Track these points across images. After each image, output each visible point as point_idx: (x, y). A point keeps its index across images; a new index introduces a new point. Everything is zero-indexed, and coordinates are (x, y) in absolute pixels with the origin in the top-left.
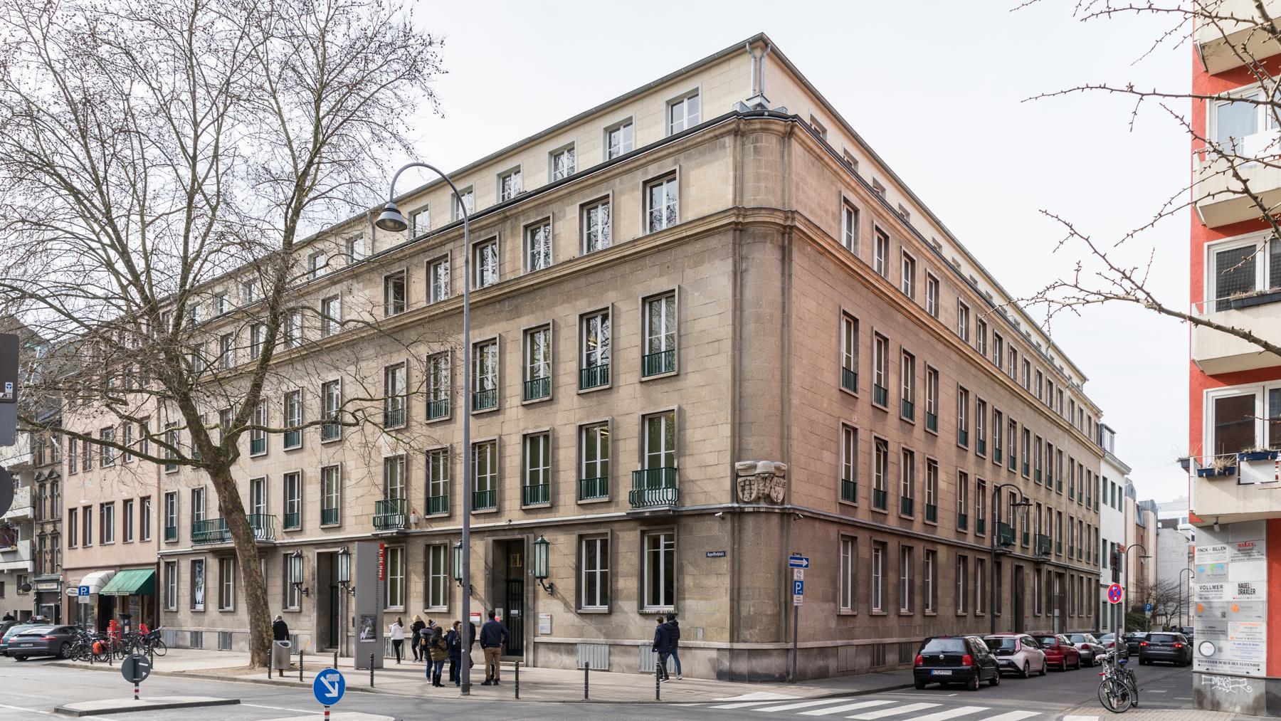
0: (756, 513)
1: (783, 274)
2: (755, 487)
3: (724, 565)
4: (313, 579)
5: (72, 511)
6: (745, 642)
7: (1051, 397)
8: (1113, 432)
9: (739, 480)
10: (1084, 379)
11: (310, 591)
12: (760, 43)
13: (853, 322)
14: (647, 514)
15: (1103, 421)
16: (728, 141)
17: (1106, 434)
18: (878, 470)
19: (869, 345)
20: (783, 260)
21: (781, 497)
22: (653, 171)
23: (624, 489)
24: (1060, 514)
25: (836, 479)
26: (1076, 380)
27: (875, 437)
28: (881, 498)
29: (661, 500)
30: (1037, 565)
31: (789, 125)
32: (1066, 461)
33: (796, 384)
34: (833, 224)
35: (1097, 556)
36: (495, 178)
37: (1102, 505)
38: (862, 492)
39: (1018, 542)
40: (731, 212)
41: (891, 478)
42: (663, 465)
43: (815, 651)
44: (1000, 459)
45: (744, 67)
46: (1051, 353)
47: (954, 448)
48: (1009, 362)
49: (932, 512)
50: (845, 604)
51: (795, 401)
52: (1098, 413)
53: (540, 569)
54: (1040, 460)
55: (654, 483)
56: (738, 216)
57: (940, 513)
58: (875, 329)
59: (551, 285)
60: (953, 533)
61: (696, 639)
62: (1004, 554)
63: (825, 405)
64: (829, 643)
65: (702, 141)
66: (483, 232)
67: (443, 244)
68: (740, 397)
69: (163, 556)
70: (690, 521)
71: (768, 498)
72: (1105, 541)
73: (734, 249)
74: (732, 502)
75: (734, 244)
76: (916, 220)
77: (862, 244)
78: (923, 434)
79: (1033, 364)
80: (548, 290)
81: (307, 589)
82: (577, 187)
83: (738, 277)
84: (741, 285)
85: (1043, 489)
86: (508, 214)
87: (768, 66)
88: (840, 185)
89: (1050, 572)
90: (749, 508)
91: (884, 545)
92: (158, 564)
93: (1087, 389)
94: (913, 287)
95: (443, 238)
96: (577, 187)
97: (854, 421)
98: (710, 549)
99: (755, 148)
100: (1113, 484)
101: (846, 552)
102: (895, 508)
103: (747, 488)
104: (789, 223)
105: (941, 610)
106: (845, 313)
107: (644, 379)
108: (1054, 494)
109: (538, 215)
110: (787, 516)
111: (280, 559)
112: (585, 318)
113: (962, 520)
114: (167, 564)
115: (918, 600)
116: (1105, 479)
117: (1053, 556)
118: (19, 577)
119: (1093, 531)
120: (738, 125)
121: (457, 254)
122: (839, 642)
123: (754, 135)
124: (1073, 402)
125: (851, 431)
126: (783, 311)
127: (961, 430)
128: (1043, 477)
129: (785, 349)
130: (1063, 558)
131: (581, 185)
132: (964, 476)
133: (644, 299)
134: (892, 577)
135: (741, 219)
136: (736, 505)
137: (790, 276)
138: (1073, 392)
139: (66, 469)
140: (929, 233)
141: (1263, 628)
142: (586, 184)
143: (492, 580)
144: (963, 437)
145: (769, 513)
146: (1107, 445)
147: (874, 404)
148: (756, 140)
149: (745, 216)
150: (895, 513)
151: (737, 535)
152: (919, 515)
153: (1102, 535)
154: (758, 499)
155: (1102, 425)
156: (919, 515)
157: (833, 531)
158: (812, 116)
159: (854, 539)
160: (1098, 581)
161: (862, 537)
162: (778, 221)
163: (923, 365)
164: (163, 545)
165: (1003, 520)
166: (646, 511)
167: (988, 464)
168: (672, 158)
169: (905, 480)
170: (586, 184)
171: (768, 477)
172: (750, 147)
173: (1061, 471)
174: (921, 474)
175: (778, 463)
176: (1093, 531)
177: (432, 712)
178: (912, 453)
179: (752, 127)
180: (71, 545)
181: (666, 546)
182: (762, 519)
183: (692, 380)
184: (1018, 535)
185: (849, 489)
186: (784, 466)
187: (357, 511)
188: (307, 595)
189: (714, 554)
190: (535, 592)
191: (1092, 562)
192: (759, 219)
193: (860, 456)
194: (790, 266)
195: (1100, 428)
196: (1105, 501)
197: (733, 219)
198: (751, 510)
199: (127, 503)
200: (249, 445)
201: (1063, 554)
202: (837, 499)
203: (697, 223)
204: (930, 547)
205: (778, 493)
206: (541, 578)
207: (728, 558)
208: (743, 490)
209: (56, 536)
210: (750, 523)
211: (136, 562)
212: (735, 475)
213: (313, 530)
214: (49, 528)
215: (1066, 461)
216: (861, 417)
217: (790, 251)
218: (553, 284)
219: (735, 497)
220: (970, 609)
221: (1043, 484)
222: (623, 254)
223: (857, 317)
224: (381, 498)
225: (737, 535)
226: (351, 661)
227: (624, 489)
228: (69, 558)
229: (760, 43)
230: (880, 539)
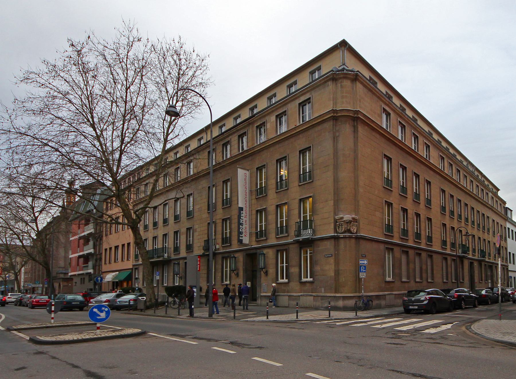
0: (345, 237)
1: (354, 137)
2: (343, 227)
3: (332, 260)
4: (183, 272)
5: (106, 250)
6: (341, 293)
7: (478, 191)
8: (512, 211)
9: (337, 223)
10: (498, 190)
11: (182, 277)
12: (344, 44)
13: (443, 191)
14: (301, 240)
15: (507, 206)
16: (330, 83)
17: (509, 212)
18: (404, 221)
19: (424, 184)
20: (354, 131)
21: (355, 231)
22: (302, 99)
23: (293, 231)
24: (489, 242)
25: (382, 223)
26: (494, 190)
27: (401, 207)
28: (405, 232)
29: (307, 234)
30: (480, 262)
31: (356, 77)
32: (491, 221)
33: (361, 183)
34: (378, 118)
35: (507, 258)
36: (248, 110)
37: (508, 239)
38: (410, 233)
39: (471, 252)
40: (331, 111)
41: (410, 224)
42: (308, 219)
43: (374, 297)
44: (474, 225)
45: (338, 55)
46: (483, 179)
47: (439, 213)
48: (481, 193)
49: (430, 239)
50: (389, 277)
51: (361, 190)
52: (505, 203)
53: (262, 264)
54: (479, 220)
55: (305, 228)
56: (334, 114)
57: (434, 240)
58: (400, 162)
59: (266, 149)
60: (440, 248)
61: (321, 292)
62: (464, 257)
63: (376, 193)
64: (381, 293)
65: (320, 84)
66: (242, 131)
67: (228, 136)
68: (337, 189)
69: (134, 265)
70: (319, 242)
71: (349, 231)
72: (510, 253)
73: (333, 128)
74: (334, 233)
75: (333, 125)
76: (420, 122)
77: (393, 127)
78: (424, 207)
79: (474, 182)
80: (265, 151)
81: (181, 277)
82: (275, 108)
83: (335, 139)
84: (337, 142)
85: (481, 231)
86: (250, 122)
87: (347, 54)
88: (381, 102)
89: (486, 265)
90: (342, 236)
91: (407, 253)
92: (132, 269)
93: (500, 194)
94: (429, 155)
95: (228, 134)
96: (275, 108)
97: (390, 200)
98: (327, 253)
99: (341, 85)
100: (512, 231)
101: (261, 226)
102: (412, 237)
103: (340, 227)
104: (356, 116)
105: (436, 280)
106: (415, 173)
107: (300, 184)
108: (486, 234)
109: (261, 122)
110: (359, 239)
111: (172, 264)
112: (279, 161)
113: (444, 243)
114: (136, 269)
115: (424, 275)
116: (509, 229)
117: (487, 258)
118: (90, 276)
119: (504, 249)
120: (333, 76)
121: (232, 140)
122: (386, 293)
123: (341, 80)
124: (493, 198)
125: (389, 205)
126: (355, 152)
127: (459, 214)
128: (481, 226)
129: (355, 168)
130: (491, 259)
131: (276, 108)
132: (444, 225)
133: (300, 152)
134: (411, 266)
135: (335, 115)
136: (336, 235)
137: (357, 138)
138: (493, 194)
139: (109, 233)
140: (427, 129)
141: (186, 138)
142: (278, 107)
143: (245, 270)
144: (443, 209)
145: (350, 237)
146: (509, 215)
147: (400, 193)
148: (342, 82)
149: (337, 113)
150: (412, 239)
151: (336, 247)
152: (423, 240)
153: (509, 251)
154: (345, 232)
155: (507, 207)
156: (423, 240)
157: (382, 247)
158: (370, 76)
159: (392, 249)
160: (507, 269)
161: (396, 249)
162: (351, 115)
163: (456, 199)
164: (134, 262)
165: (482, 249)
166: (300, 238)
167: (447, 217)
168: (309, 93)
169: (417, 225)
170: (278, 107)
171: (349, 222)
172: (339, 85)
173: (489, 225)
174: (424, 224)
175: (353, 216)
176: (504, 249)
177: (447, 316)
178: (407, 210)
179: (339, 76)
180: (105, 263)
181: (310, 253)
182: (347, 241)
183: (317, 183)
184: (471, 249)
185: (389, 228)
186: (357, 217)
187: (199, 245)
188: (181, 279)
189: (328, 256)
190: (261, 274)
191: (504, 261)
192: (343, 114)
193: (394, 215)
194: (357, 133)
195: (507, 209)
196: (509, 237)
197: (332, 115)
198: (342, 236)
199: (123, 245)
200: (162, 221)
201: (491, 258)
202: (400, 236)
203: (319, 118)
204: (430, 254)
205: (354, 229)
206: (262, 269)
207: (333, 257)
208: (339, 228)
209: (101, 259)
210: (342, 242)
211: (125, 268)
212: (336, 221)
213: (183, 253)
214: (99, 256)
215: (491, 221)
216: (394, 198)
217: (357, 128)
218: (267, 148)
219: (336, 231)
220: (450, 279)
221: (481, 229)
222: (291, 134)
223: (419, 174)
224: (206, 239)
225: (336, 247)
226: (172, 305)
227: (293, 231)
228: (104, 268)
229: (344, 44)
230: (405, 250)
